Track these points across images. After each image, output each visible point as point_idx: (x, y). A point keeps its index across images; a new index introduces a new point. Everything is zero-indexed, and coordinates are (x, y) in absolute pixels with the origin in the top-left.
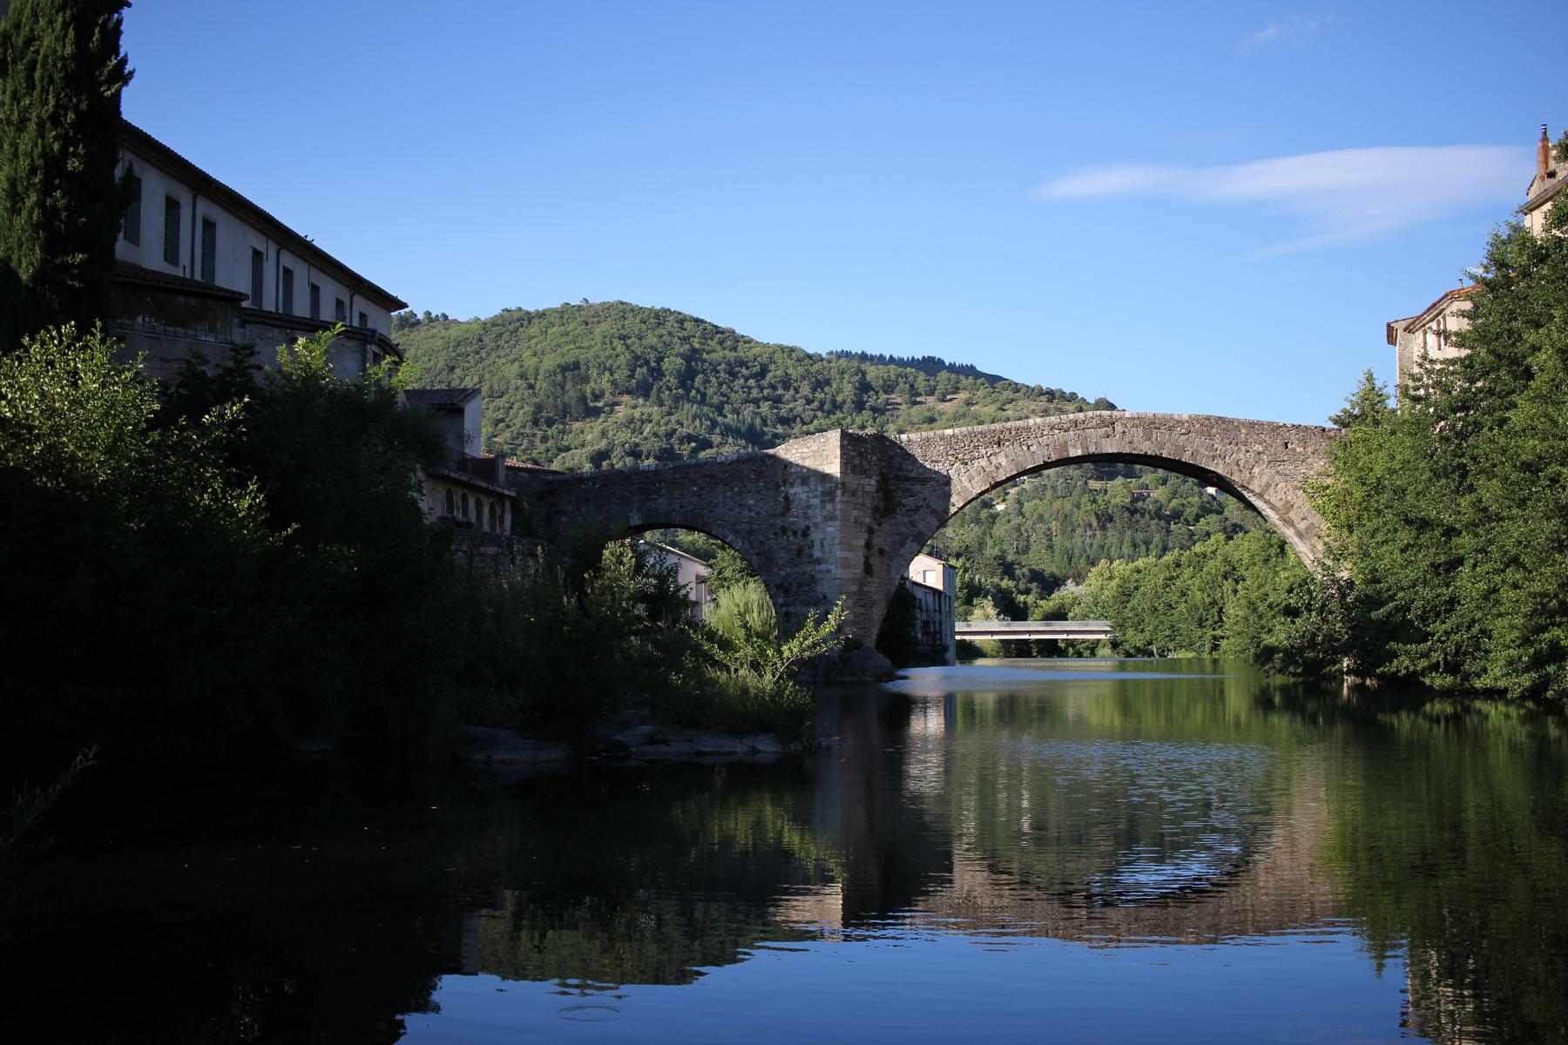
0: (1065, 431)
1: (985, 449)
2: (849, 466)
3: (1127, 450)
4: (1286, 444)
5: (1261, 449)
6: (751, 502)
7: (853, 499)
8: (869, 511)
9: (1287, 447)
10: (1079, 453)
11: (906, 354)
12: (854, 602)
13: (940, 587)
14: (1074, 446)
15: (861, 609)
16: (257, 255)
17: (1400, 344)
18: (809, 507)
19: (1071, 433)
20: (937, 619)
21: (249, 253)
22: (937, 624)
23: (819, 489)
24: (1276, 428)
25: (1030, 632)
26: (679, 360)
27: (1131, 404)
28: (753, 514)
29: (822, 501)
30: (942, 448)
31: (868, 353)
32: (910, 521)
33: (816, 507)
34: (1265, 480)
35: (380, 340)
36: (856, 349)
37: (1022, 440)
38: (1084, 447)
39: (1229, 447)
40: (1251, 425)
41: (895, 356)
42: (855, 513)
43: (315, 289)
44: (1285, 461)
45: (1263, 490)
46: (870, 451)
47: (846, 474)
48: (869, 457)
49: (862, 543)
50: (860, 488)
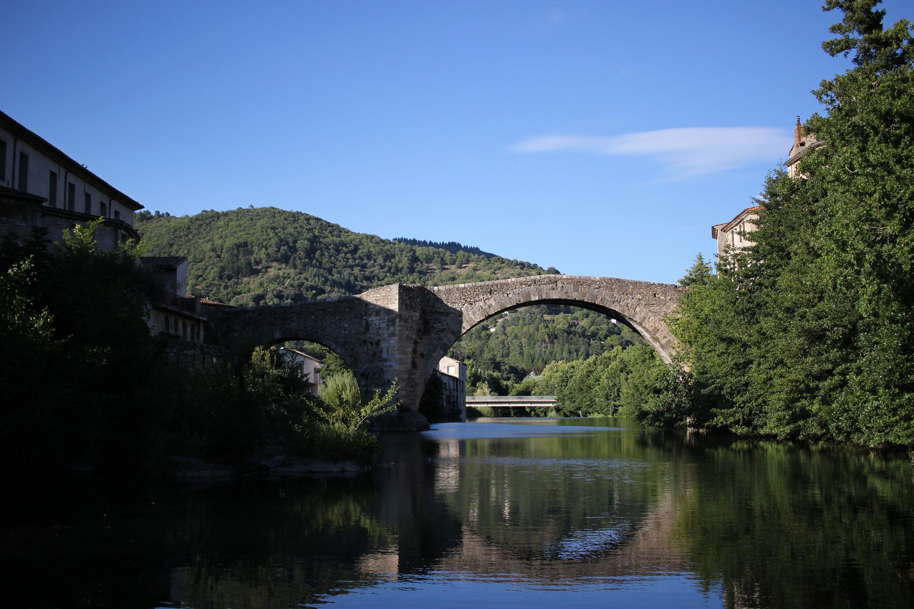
0: (529, 286)
1: (483, 295)
2: (404, 305)
3: (564, 297)
4: (655, 294)
5: (640, 297)
6: (346, 325)
8: (415, 331)
9: (655, 296)
10: (537, 298)
11: (439, 241)
12: (406, 384)
13: (457, 376)
15: (410, 388)
16: (53, 175)
17: (719, 238)
18: (380, 328)
19: (532, 287)
20: (455, 395)
21: (48, 175)
22: (455, 398)
23: (386, 318)
24: (649, 285)
25: (509, 403)
26: (306, 242)
27: (569, 270)
28: (347, 332)
29: (387, 325)
30: (458, 295)
31: (417, 239)
33: (384, 329)
34: (643, 315)
35: (126, 227)
36: (410, 237)
37: (504, 291)
38: (540, 295)
39: (622, 296)
40: (635, 284)
41: (433, 242)
42: (407, 332)
43: (88, 196)
44: (654, 304)
45: (641, 321)
46: (416, 296)
47: (402, 309)
48: (415, 300)
49: (410, 350)
50: (410, 318)
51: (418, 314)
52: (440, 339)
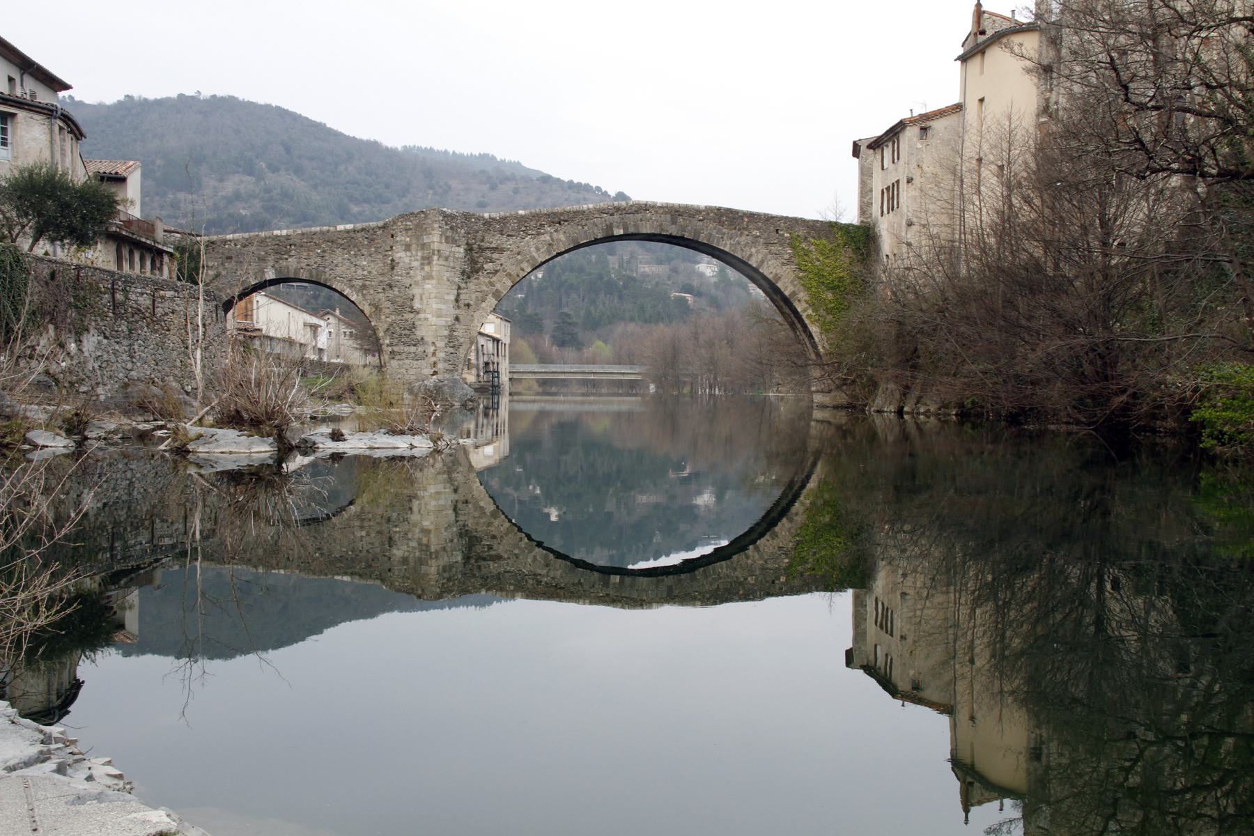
3: (658, 231)
6: (365, 263)
7: (444, 263)
10: (621, 232)
14: (618, 227)
28: (365, 273)
29: (422, 264)
32: (490, 282)
35: (62, 114)
38: (625, 228)
40: (752, 216)
42: (448, 274)
49: (452, 297)
51: (462, 250)
52: (492, 284)
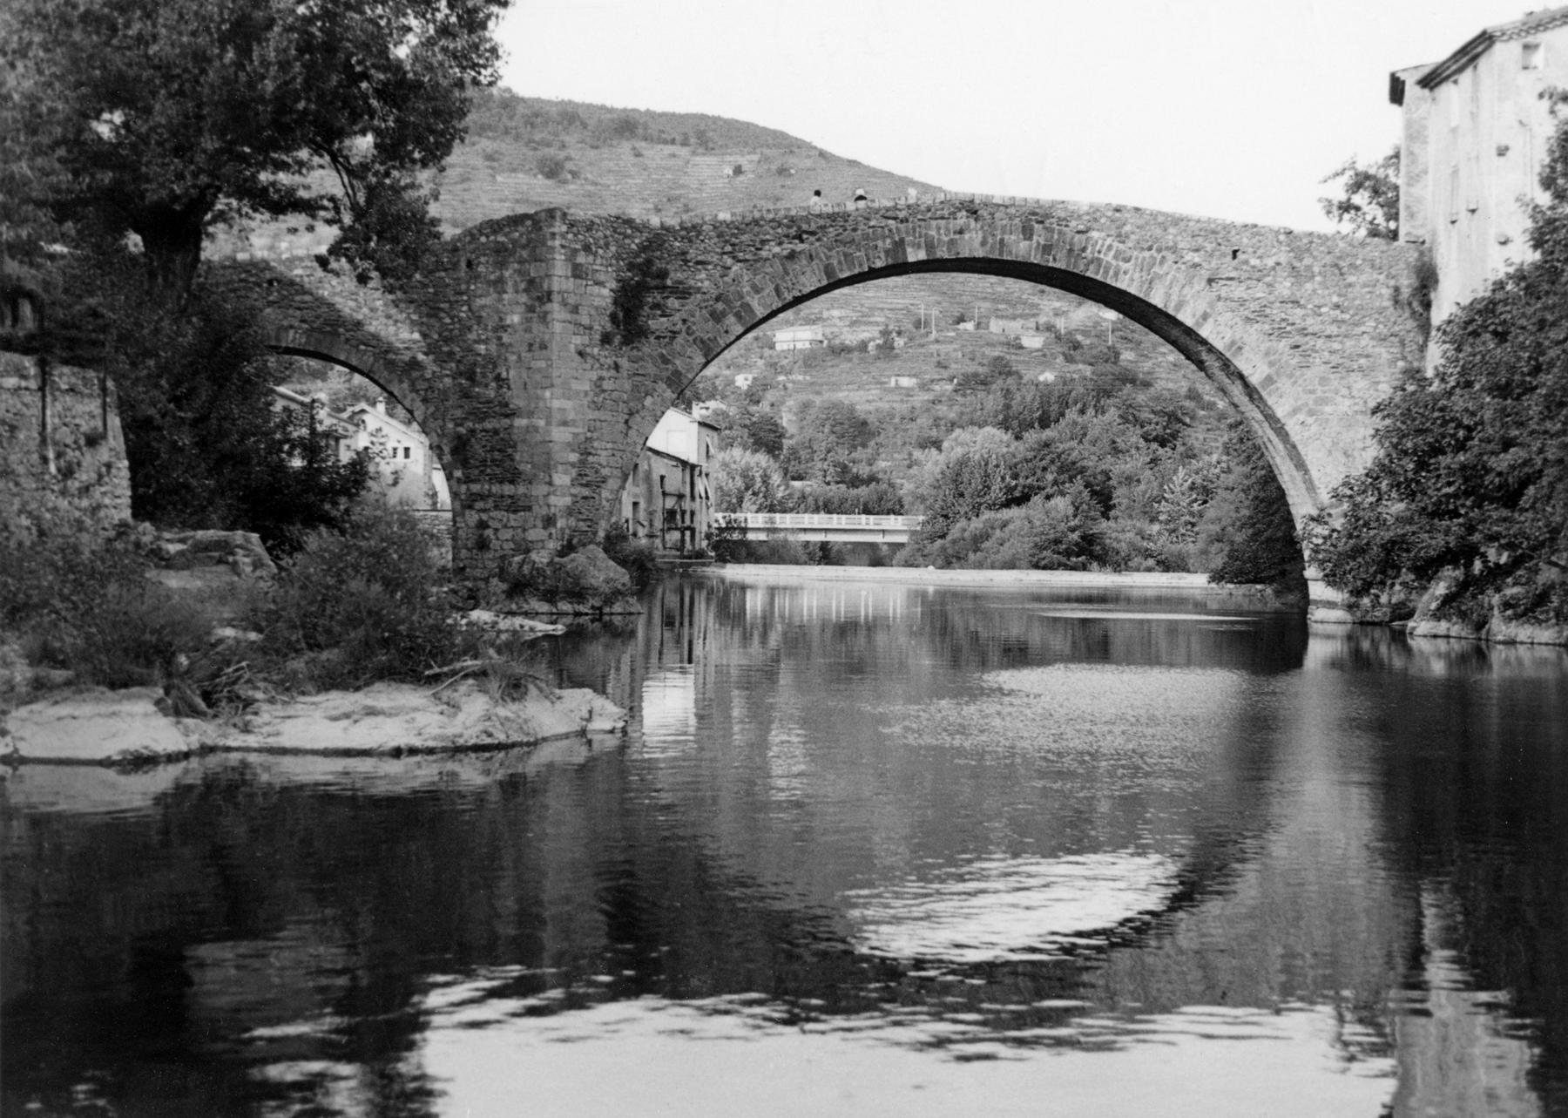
4: (1235, 253)
10: (922, 255)
22: (687, 517)
